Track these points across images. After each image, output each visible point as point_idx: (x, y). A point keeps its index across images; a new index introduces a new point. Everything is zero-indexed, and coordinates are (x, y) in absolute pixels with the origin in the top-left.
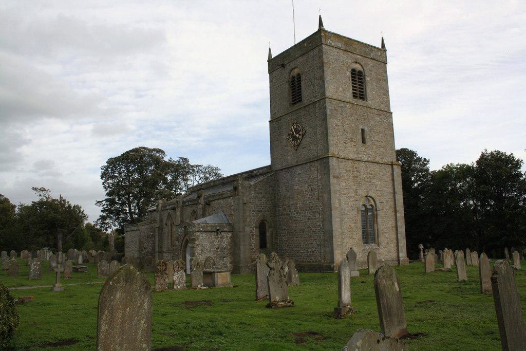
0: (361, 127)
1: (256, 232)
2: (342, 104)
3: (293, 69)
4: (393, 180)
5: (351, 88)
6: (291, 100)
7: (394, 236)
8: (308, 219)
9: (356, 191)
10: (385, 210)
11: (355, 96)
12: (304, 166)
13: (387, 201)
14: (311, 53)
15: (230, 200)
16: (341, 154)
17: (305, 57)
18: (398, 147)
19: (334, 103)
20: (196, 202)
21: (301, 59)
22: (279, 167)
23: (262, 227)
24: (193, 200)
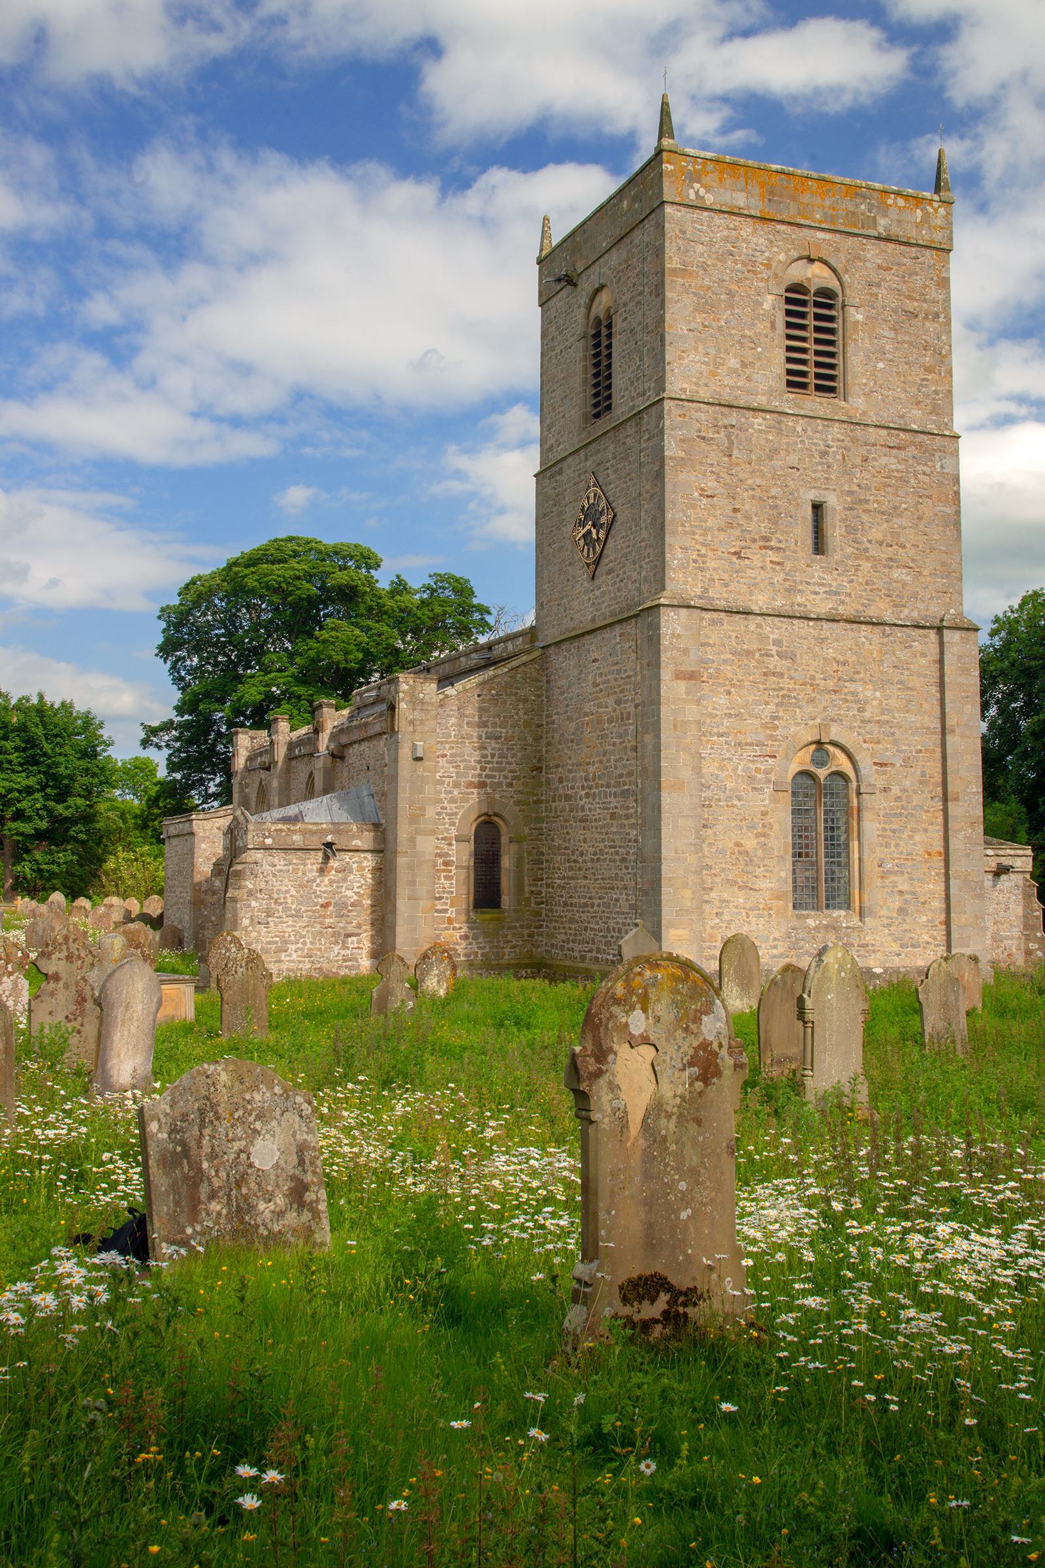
0: (812, 495)
2: (733, 418)
5: (780, 355)
7: (942, 887)
8: (613, 816)
10: (896, 790)
11: (795, 382)
12: (607, 634)
13: (906, 760)
19: (704, 415)
21: (614, 258)
22: (550, 634)
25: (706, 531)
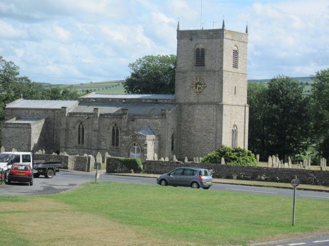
14: (214, 40)
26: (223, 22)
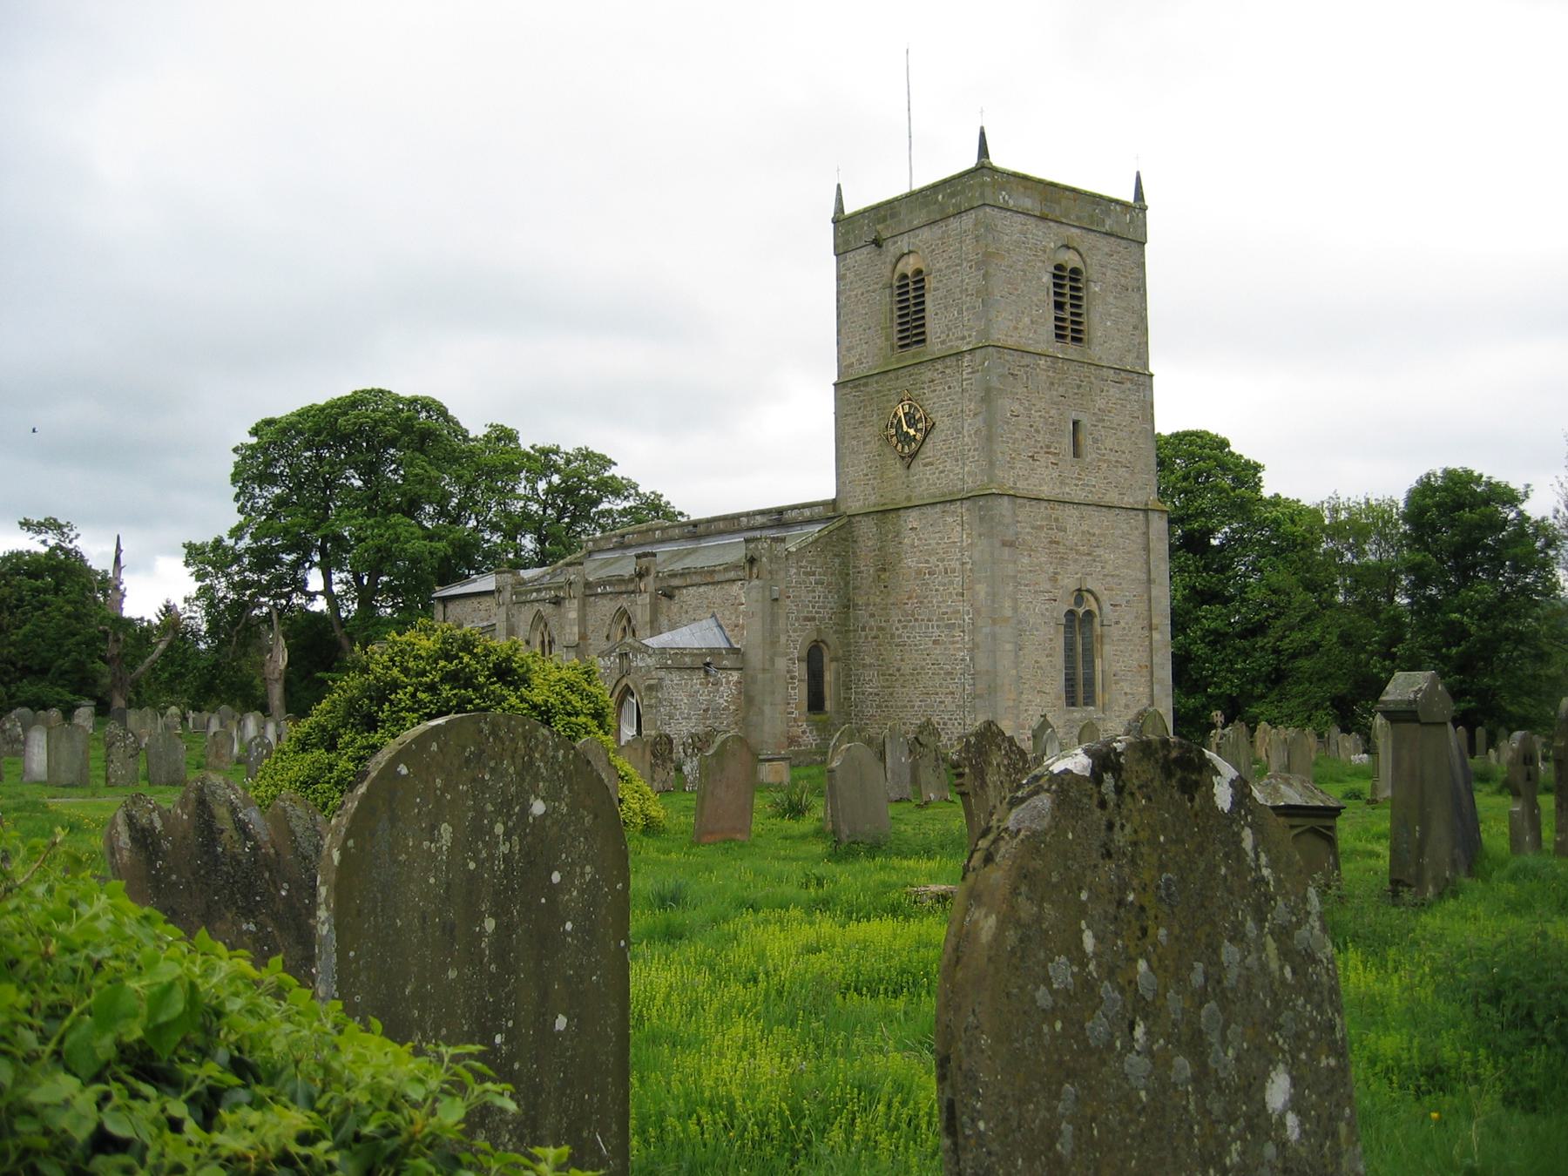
0: (1074, 415)
1: (800, 670)
2: (1027, 360)
3: (903, 255)
4: (1147, 549)
6: (897, 336)
9: (1053, 579)
10: (1122, 624)
12: (929, 510)
14: (954, 224)
15: (736, 587)
16: (1023, 487)
17: (937, 230)
18: (1166, 424)
20: (631, 587)
21: (925, 234)
23: (814, 659)
24: (621, 580)
25: (1015, 441)
26: (982, 135)
